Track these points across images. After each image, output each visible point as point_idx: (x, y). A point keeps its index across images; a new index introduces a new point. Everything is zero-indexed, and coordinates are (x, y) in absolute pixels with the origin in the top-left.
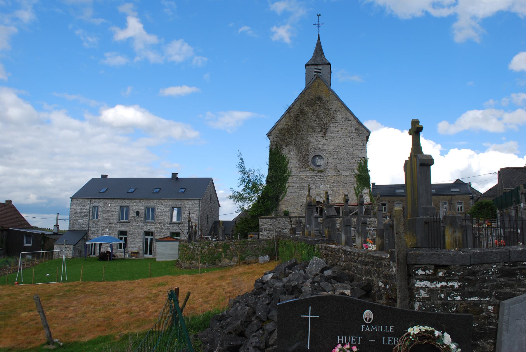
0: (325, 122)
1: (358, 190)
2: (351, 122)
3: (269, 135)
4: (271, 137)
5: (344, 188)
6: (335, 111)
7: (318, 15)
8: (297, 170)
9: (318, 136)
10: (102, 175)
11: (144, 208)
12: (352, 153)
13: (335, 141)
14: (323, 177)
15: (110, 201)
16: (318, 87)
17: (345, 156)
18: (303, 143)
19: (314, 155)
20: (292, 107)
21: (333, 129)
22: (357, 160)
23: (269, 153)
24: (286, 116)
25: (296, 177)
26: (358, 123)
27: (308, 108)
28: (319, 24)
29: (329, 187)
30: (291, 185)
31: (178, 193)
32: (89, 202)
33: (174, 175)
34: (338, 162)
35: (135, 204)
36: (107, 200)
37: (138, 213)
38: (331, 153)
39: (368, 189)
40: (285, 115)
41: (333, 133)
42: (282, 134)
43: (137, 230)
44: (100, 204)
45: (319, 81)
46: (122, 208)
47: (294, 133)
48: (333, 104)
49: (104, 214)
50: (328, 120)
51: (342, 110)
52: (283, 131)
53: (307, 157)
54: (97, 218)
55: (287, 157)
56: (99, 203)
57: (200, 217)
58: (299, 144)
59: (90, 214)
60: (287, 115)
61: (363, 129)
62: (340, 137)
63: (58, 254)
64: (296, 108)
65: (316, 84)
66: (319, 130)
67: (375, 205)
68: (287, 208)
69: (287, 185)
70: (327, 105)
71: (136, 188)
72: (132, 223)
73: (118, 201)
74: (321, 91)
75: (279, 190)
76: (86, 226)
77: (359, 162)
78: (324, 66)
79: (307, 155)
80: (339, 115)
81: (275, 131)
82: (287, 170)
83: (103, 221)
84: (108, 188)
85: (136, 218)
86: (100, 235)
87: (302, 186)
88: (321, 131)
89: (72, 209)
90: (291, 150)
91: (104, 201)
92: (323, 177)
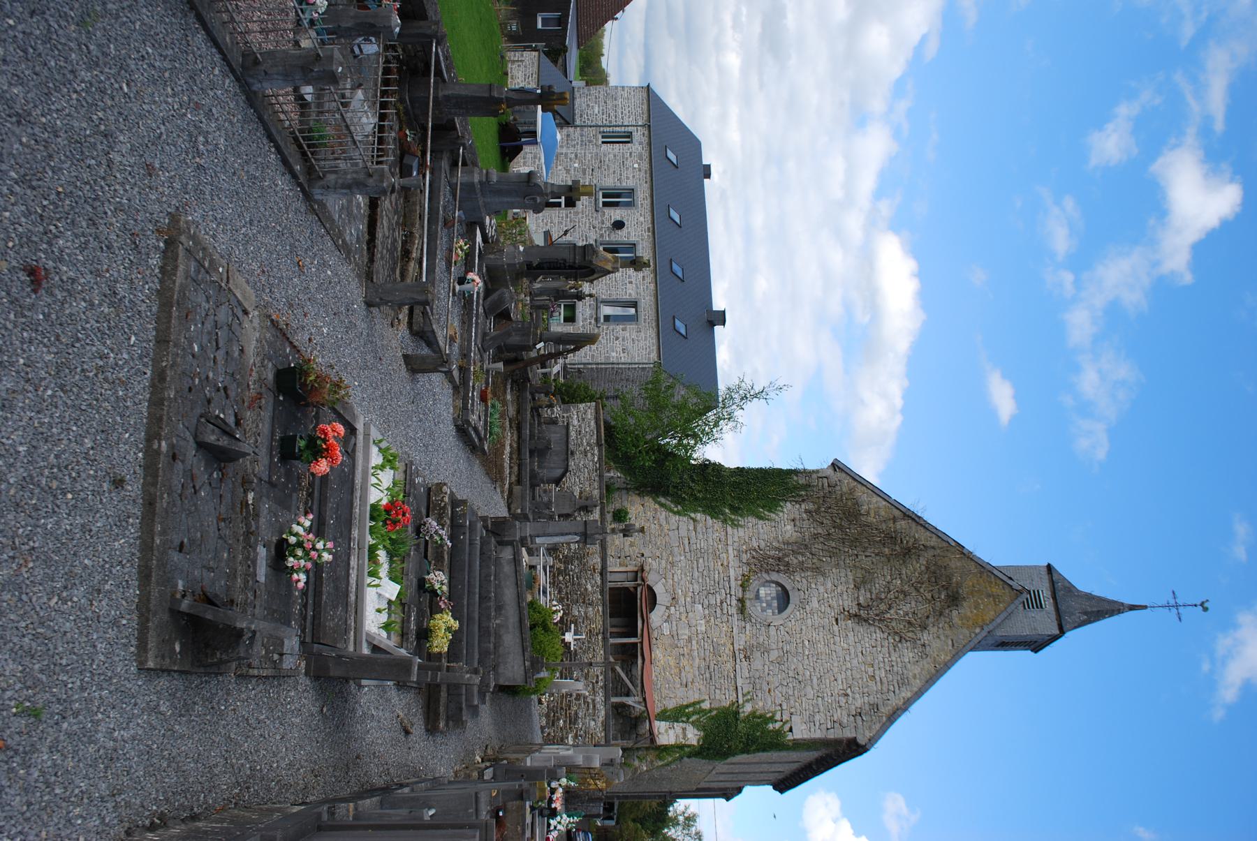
0: (888, 615)
1: (694, 713)
2: (894, 692)
3: (836, 466)
4: (830, 472)
5: (697, 673)
6: (924, 645)
7: (1206, 605)
8: (743, 542)
9: (845, 597)
10: (709, 166)
11: (633, 239)
12: (803, 693)
13: (833, 647)
14: (725, 612)
15: (646, 166)
16: (989, 596)
17: (791, 674)
18: (821, 558)
19: (788, 587)
20: (921, 525)
21: (870, 638)
22: (782, 710)
23: (785, 467)
24: (895, 510)
25: (723, 538)
26: (894, 713)
27: (923, 568)
28: (1177, 606)
29: (699, 628)
30: (700, 526)
31: (674, 317)
32: (640, 123)
33: (720, 318)
34: (774, 655)
35: (642, 219)
36: (647, 160)
37: (619, 225)
38: (799, 636)
39: (698, 742)
40: (896, 505)
41: (857, 640)
42: (842, 500)
43: (579, 226)
44: (638, 145)
45: (1007, 599)
46: (631, 193)
47: (848, 530)
48: (942, 638)
49: (615, 156)
50: (894, 624)
51: (927, 665)
52: (849, 503)
53: (782, 568)
54: (603, 142)
55: (777, 515)
56: (640, 143)
57: (615, 366)
58: (816, 546)
59: (613, 126)
60: (897, 513)
61: (878, 726)
62: (848, 659)
63: (518, 61)
64: (922, 535)
65: (995, 590)
66: (862, 600)
67: (652, 762)
68: (634, 518)
69: (699, 516)
70: (937, 620)
71: (680, 227)
72: (595, 215)
73: (646, 182)
74: (979, 604)
75: (685, 493)
76: (584, 122)
77: (778, 717)
78: (1053, 616)
79: (788, 569)
80: (911, 655)
81: (847, 480)
82: (741, 516)
83: (597, 154)
84: (680, 227)
85: (608, 224)
86: (564, 152)
87: (699, 556)
88: (859, 604)
89: (623, 90)
90: (797, 523)
91: (646, 155)
92: (725, 612)
